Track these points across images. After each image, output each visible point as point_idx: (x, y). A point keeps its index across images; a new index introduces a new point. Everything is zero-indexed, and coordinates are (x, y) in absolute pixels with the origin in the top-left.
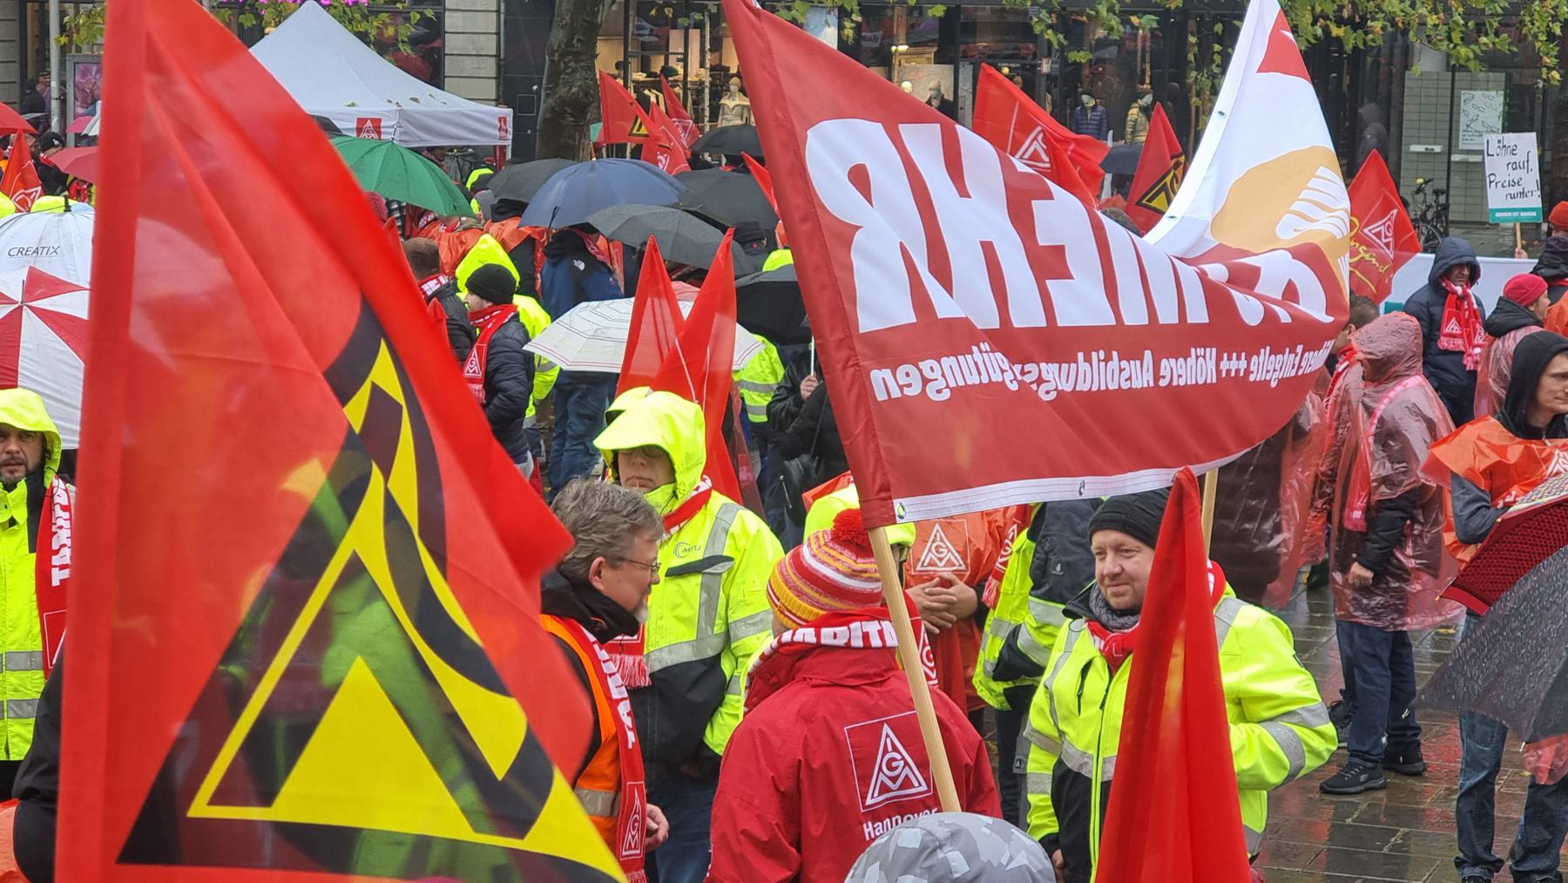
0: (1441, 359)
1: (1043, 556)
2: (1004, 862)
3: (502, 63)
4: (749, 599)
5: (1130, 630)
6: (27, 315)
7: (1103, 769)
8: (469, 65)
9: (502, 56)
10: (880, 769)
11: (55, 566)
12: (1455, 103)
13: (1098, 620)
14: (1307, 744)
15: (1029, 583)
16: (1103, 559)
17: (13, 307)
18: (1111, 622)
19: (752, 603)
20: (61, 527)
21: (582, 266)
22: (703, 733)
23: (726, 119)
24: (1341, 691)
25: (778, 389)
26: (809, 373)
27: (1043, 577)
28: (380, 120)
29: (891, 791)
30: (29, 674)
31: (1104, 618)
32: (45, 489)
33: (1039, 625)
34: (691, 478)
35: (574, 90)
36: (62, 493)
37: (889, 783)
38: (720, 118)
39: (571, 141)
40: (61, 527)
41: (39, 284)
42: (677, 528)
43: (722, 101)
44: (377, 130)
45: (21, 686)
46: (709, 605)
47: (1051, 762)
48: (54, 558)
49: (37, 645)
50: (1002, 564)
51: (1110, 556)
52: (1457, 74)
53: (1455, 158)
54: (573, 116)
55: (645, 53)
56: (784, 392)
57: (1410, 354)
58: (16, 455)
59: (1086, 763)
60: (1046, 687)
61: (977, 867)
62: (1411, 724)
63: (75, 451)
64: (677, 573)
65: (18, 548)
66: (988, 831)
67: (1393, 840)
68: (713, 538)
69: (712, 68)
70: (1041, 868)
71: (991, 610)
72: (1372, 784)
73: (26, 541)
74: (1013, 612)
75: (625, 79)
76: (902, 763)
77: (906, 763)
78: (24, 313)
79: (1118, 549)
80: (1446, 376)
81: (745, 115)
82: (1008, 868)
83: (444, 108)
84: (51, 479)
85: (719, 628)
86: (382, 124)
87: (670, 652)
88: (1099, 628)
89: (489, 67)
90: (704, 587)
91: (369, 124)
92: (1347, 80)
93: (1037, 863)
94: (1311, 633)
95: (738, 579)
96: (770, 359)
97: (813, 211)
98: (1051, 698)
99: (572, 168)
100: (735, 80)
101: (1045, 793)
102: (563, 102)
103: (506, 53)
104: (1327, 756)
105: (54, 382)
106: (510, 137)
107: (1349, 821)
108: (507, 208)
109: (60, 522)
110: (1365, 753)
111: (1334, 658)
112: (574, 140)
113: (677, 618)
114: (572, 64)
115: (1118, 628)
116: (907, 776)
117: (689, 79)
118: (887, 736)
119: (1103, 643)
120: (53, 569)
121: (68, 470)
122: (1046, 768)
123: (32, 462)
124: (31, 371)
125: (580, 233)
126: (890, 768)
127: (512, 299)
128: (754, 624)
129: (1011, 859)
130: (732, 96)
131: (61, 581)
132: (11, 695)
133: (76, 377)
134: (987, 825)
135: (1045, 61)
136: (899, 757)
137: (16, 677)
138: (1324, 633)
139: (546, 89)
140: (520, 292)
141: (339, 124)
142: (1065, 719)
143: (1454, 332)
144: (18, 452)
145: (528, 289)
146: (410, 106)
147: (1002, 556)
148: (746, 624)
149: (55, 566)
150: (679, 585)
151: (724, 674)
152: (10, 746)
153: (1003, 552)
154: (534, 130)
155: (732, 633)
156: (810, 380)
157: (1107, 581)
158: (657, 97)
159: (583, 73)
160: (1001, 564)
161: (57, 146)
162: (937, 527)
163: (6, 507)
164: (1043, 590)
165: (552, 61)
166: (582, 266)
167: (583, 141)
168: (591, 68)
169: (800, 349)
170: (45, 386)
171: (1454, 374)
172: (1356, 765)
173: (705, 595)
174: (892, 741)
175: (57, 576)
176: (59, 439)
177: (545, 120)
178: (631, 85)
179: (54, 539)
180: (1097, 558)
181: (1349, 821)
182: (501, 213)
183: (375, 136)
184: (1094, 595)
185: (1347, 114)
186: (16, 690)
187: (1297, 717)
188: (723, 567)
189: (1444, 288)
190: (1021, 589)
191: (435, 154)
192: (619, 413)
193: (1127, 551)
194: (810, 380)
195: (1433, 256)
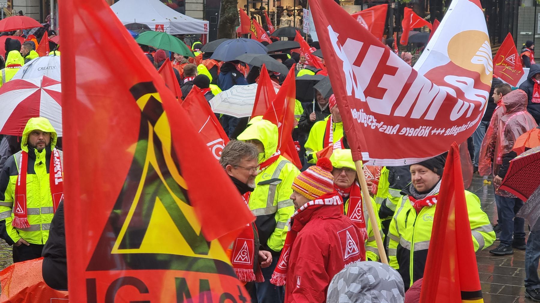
0: (533, 106)
1: (392, 174)
2: (387, 278)
3: (205, 5)
4: (285, 194)
5: (423, 199)
6: (42, 91)
7: (414, 247)
8: (194, 6)
9: (205, 3)
11: (56, 178)
12: (536, 17)
13: (412, 196)
14: (485, 238)
15: (388, 184)
16: (414, 175)
17: (38, 89)
18: (417, 196)
19: (286, 196)
20: (57, 164)
21: (235, 75)
22: (267, 242)
23: (282, 25)
24: (498, 221)
25: (302, 117)
26: (313, 112)
27: (393, 181)
28: (163, 25)
30: (49, 215)
31: (414, 195)
32: (51, 151)
33: (393, 198)
34: (271, 150)
35: (230, 14)
36: (57, 153)
37: (242, 258)
38: (280, 24)
39: (229, 32)
40: (57, 164)
41: (46, 81)
42: (264, 168)
43: (281, 19)
44: (162, 28)
45: (46, 219)
46: (271, 196)
47: (396, 245)
48: (55, 175)
49: (51, 205)
50: (377, 179)
51: (417, 173)
52: (537, 7)
53: (536, 36)
54: (230, 24)
55: (254, 2)
56: (303, 118)
57: (520, 104)
58: (42, 140)
59: (409, 245)
60: (394, 219)
61: (378, 280)
62: (522, 232)
63: (61, 137)
64: (262, 184)
65: (43, 172)
66: (381, 268)
67: (516, 272)
68: (276, 172)
69: (277, 7)
70: (400, 280)
71: (375, 195)
72: (508, 252)
73: (46, 169)
74: (383, 195)
75: (248, 11)
76: (352, 243)
77: (353, 244)
78: (41, 91)
79: (420, 171)
80: (535, 112)
81: (289, 23)
82: (389, 281)
83: (185, 21)
84: (54, 149)
85: (274, 204)
86: (164, 27)
87: (256, 212)
88: (413, 198)
89: (201, 7)
90: (270, 189)
91: (160, 27)
92: (498, 9)
93: (397, 278)
94: (488, 201)
95: (282, 187)
96: (299, 106)
98: (396, 222)
99: (229, 41)
100: (285, 11)
101: (394, 255)
102: (227, 19)
103: (206, 3)
104: (492, 242)
105: (52, 114)
106: (208, 31)
107: (500, 265)
108: (207, 55)
109: (57, 163)
110: (506, 241)
111: (495, 210)
112: (230, 32)
113: (260, 200)
114: (230, 6)
115: (419, 198)
117: (270, 11)
118: (245, 245)
119: (414, 203)
120: (55, 179)
121: (59, 146)
122: (395, 247)
123: (47, 143)
124: (44, 111)
125: (233, 64)
126: (350, 246)
127: (209, 86)
128: (286, 203)
129: (389, 277)
130: (284, 17)
131: (59, 183)
132: (43, 222)
133: (59, 113)
134: (381, 266)
135: (393, 4)
136: (351, 241)
137: (45, 216)
138: (492, 200)
139: (221, 14)
140: (212, 83)
141: (150, 27)
142: (401, 230)
143: (537, 96)
144: (43, 139)
145: (214, 83)
146: (173, 20)
147: (377, 176)
148: (283, 203)
149: (56, 178)
150: (262, 188)
151: (275, 220)
152: (43, 240)
153: (377, 175)
154: (216, 28)
155: (278, 206)
156: (313, 114)
157: (416, 182)
158: (259, 17)
159: (233, 9)
160: (377, 179)
161: (54, 35)
163: (38, 158)
164: (393, 186)
165: (223, 5)
166: (235, 75)
167: (233, 32)
168: (236, 7)
169: (309, 103)
170: (49, 116)
171: (538, 111)
172: (503, 246)
173: (270, 192)
175: (57, 182)
176: (56, 134)
177: (220, 25)
178: (250, 13)
179: (55, 168)
180: (412, 174)
181: (500, 265)
182: (206, 57)
183: (162, 31)
184: (411, 187)
185: (498, 22)
186: (45, 220)
187: (482, 229)
188: (277, 183)
189: (533, 81)
190: (385, 186)
191: (181, 37)
192: (251, 124)
193: (423, 171)
194: (313, 114)
195: (529, 69)
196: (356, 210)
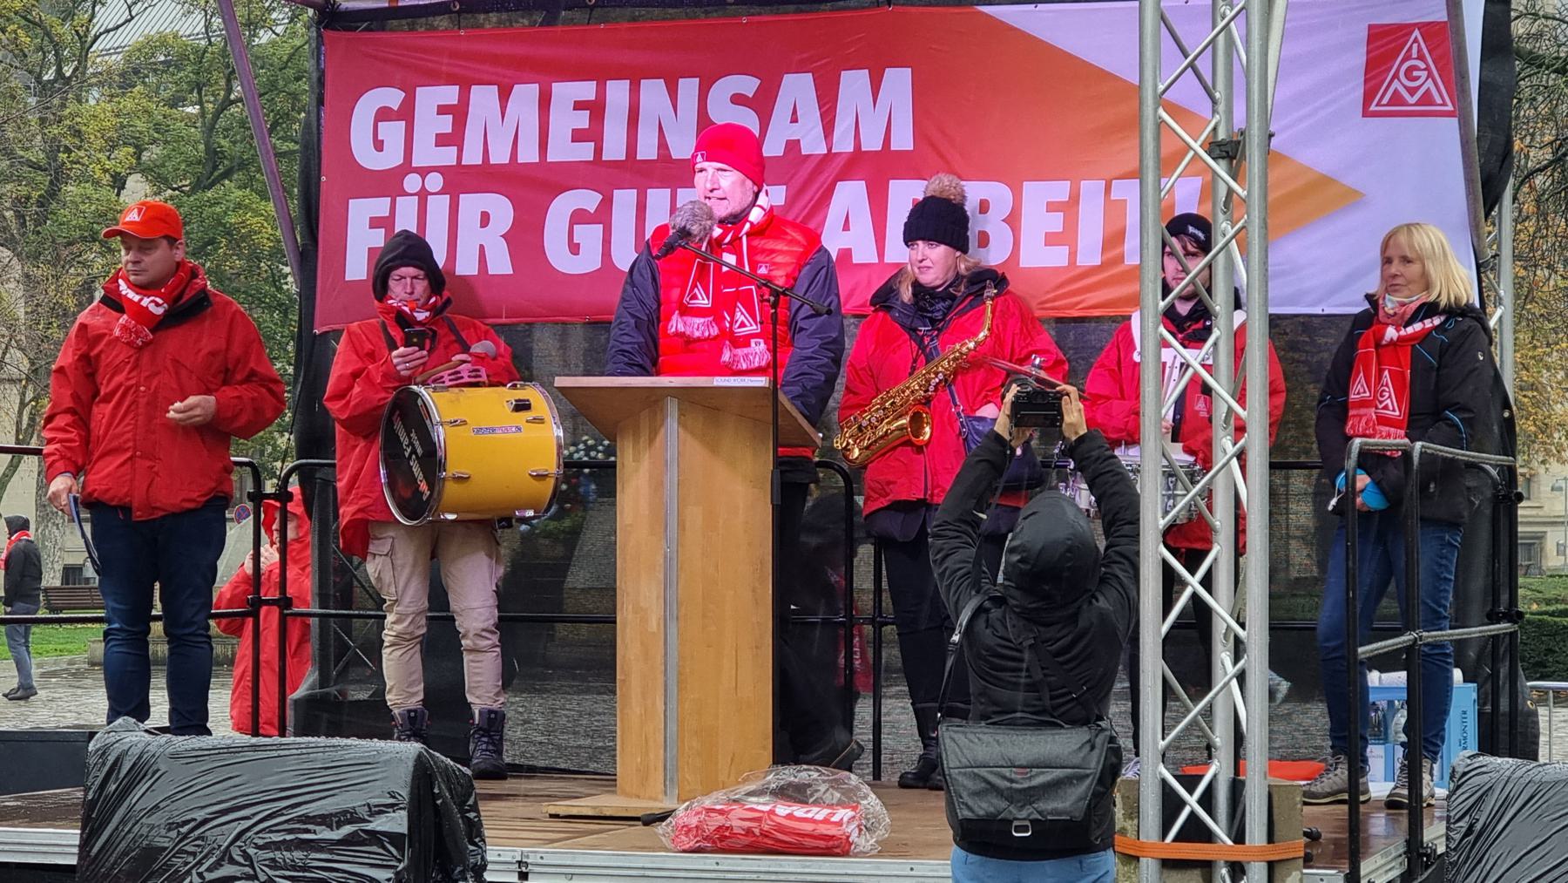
10: (1396, 76)
29: (1405, 103)
77: (1430, 75)
97: (269, 415)
116: (1428, 90)
118: (1416, 40)
162: (1417, 33)
174: (1419, 46)
196: (1405, 87)
